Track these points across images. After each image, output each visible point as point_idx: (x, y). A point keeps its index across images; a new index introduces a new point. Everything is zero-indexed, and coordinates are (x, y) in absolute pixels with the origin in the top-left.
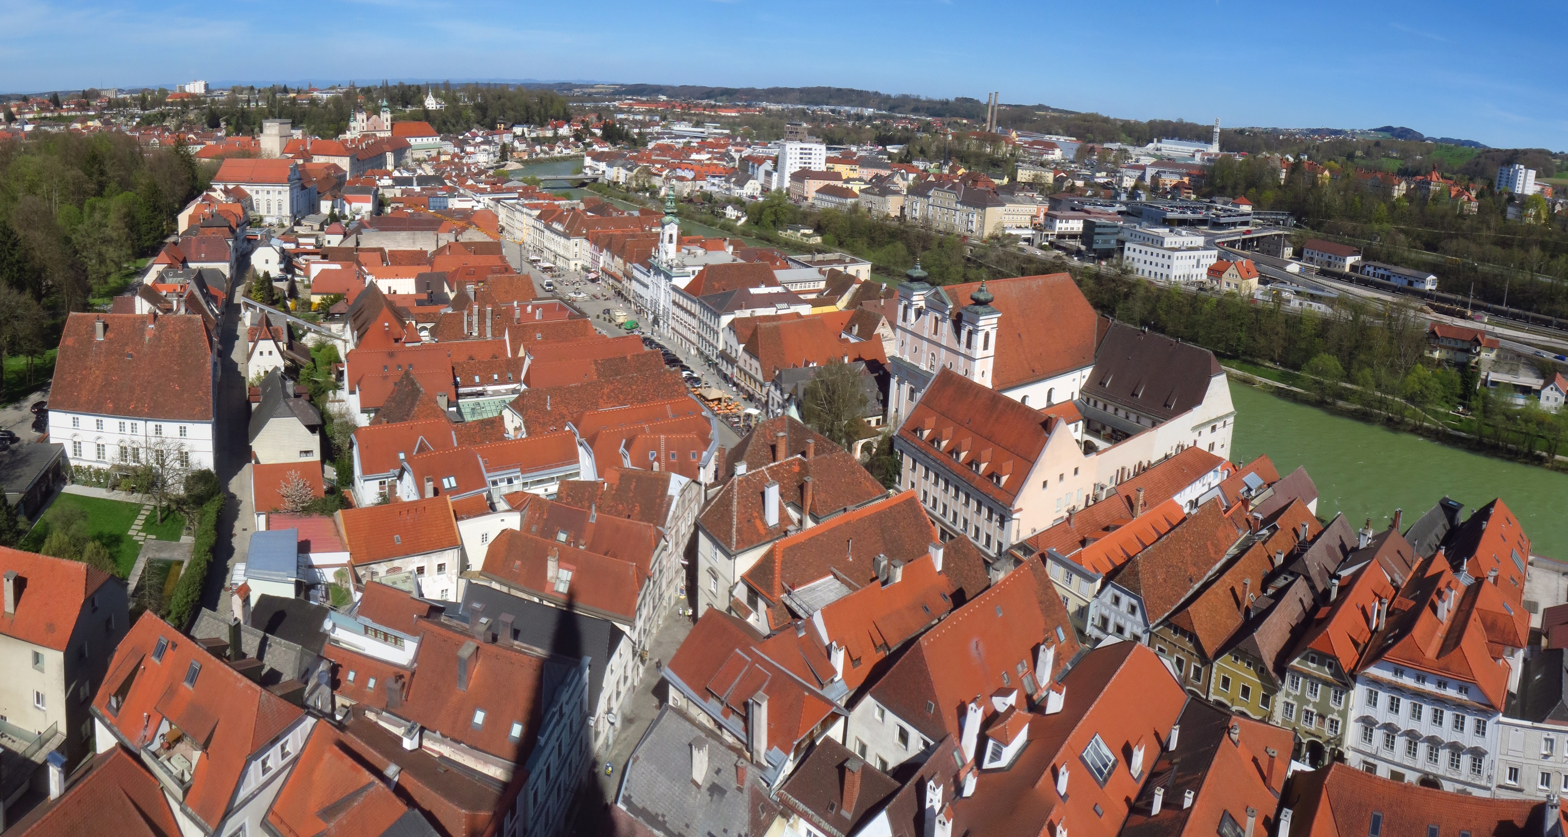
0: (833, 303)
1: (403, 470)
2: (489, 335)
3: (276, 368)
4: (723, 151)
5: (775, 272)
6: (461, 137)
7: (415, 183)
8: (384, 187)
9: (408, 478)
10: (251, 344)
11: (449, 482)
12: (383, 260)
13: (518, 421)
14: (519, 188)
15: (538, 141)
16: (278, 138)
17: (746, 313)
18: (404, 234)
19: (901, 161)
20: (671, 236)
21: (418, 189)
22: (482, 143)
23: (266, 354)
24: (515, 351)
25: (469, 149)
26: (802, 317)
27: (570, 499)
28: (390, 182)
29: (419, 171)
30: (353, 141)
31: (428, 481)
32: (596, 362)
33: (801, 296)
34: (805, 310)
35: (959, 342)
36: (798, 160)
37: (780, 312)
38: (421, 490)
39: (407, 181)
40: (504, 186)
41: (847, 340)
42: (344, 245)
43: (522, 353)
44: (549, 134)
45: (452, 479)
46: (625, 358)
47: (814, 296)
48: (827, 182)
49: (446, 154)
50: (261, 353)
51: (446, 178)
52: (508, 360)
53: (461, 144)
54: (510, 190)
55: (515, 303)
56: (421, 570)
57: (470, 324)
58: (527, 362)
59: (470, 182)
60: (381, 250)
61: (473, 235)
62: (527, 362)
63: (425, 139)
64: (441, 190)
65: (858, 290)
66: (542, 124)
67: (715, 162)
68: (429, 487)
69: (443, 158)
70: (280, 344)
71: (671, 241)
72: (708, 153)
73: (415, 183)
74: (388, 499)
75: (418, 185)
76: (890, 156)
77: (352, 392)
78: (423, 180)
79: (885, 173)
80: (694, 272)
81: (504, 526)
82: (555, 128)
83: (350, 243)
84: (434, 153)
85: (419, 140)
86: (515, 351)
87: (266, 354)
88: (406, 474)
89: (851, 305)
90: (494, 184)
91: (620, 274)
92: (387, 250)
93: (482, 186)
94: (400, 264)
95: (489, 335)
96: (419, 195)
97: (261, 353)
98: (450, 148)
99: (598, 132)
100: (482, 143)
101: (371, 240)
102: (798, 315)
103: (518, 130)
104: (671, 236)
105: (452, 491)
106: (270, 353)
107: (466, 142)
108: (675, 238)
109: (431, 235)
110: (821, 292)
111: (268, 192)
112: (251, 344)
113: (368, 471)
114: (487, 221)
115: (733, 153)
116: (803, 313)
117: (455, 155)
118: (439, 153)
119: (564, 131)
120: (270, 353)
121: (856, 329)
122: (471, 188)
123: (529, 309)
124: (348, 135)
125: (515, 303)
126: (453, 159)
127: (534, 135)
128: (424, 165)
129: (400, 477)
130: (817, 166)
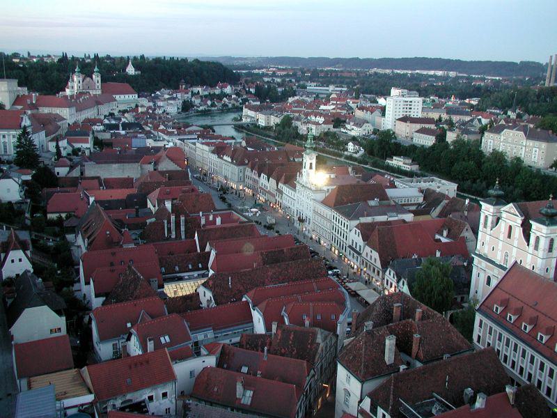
0: (428, 213)
1: (130, 334)
2: (183, 237)
3: (26, 272)
4: (344, 103)
5: (386, 190)
6: (153, 95)
7: (121, 128)
8: (98, 131)
9: (134, 339)
10: (3, 255)
11: (165, 339)
12: (101, 185)
13: (209, 294)
14: (198, 131)
15: (212, 97)
16: (7, 94)
17: (369, 220)
18: (115, 166)
19: (478, 110)
20: (311, 164)
21: (123, 132)
22: (169, 99)
23: (17, 261)
24: (203, 248)
25: (160, 103)
26: (406, 223)
27: (248, 346)
28: (102, 128)
29: (123, 120)
30: (72, 97)
31: (150, 340)
32: (262, 254)
33: (405, 207)
34: (409, 217)
35: (528, 245)
36: (401, 110)
37: (390, 219)
38: (144, 346)
39: (116, 127)
40: (187, 130)
41: (440, 240)
42: (70, 175)
43: (207, 249)
44: (217, 91)
45: (167, 338)
46: (282, 250)
47: (414, 208)
48: (423, 125)
49: (142, 106)
50: (13, 261)
51: (144, 124)
52: (199, 254)
53: (153, 100)
54: (191, 133)
55: (201, 214)
56: (151, 398)
57: (169, 230)
58: (213, 253)
59: (162, 127)
60: (98, 178)
61: (167, 165)
62: (213, 253)
63: (127, 96)
64: (140, 133)
65: (447, 204)
66: (213, 86)
67: (339, 111)
68: (151, 346)
69: (140, 110)
70: (28, 253)
71: (311, 168)
72: (333, 104)
73: (121, 128)
74: (120, 354)
75: (123, 129)
76: (472, 106)
77: (87, 283)
78: (125, 126)
79: (467, 118)
80: (328, 190)
81: (205, 365)
82: (221, 88)
83: (76, 173)
84: (133, 106)
85: (122, 96)
86: (203, 248)
87: (17, 261)
88: (133, 336)
89: (441, 215)
90: (179, 129)
91: (275, 193)
92: (102, 178)
93: (170, 130)
94: (113, 188)
95: (183, 237)
96: (125, 136)
97: (13, 261)
98: (145, 102)
99: (252, 90)
100: (169, 99)
101: (92, 170)
102: (404, 221)
103: (196, 89)
104: (311, 164)
105: (167, 345)
106: (20, 260)
107: (157, 97)
108: (314, 166)
109: (136, 165)
110: (419, 205)
111: (4, 136)
112: (3, 255)
113: (103, 338)
114: (176, 155)
115: (351, 104)
116: (407, 220)
117: (150, 108)
118: (137, 106)
119: (228, 90)
120: (20, 260)
121: (445, 233)
122: (162, 131)
123: (211, 218)
124: (68, 92)
125: (201, 214)
126: (148, 110)
127: (206, 93)
128: (126, 115)
129: (129, 339)
130: (416, 114)
